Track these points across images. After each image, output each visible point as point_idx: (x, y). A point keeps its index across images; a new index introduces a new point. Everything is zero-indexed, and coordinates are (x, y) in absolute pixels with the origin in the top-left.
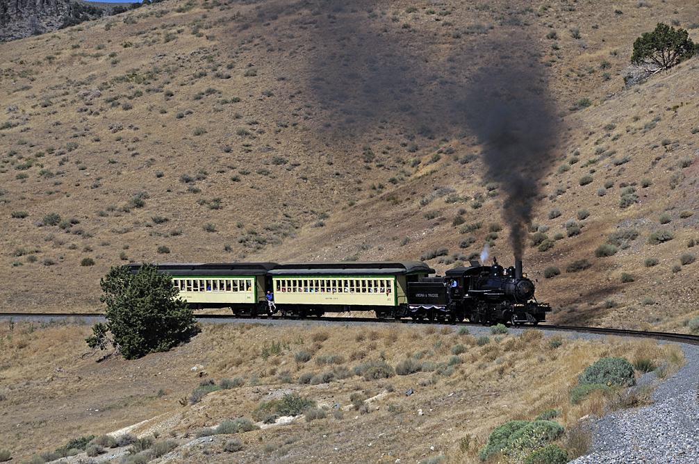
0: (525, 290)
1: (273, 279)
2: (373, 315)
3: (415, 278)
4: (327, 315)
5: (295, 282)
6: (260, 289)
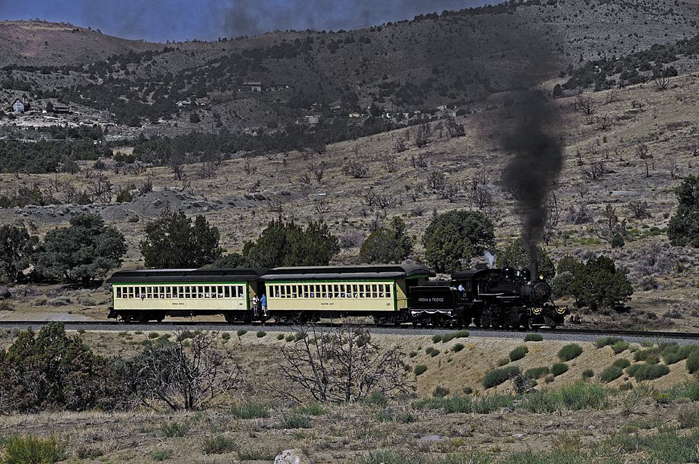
0: (541, 292)
1: (266, 284)
2: (370, 320)
3: (415, 282)
4: (167, 319)
5: (312, 287)
6: (253, 293)
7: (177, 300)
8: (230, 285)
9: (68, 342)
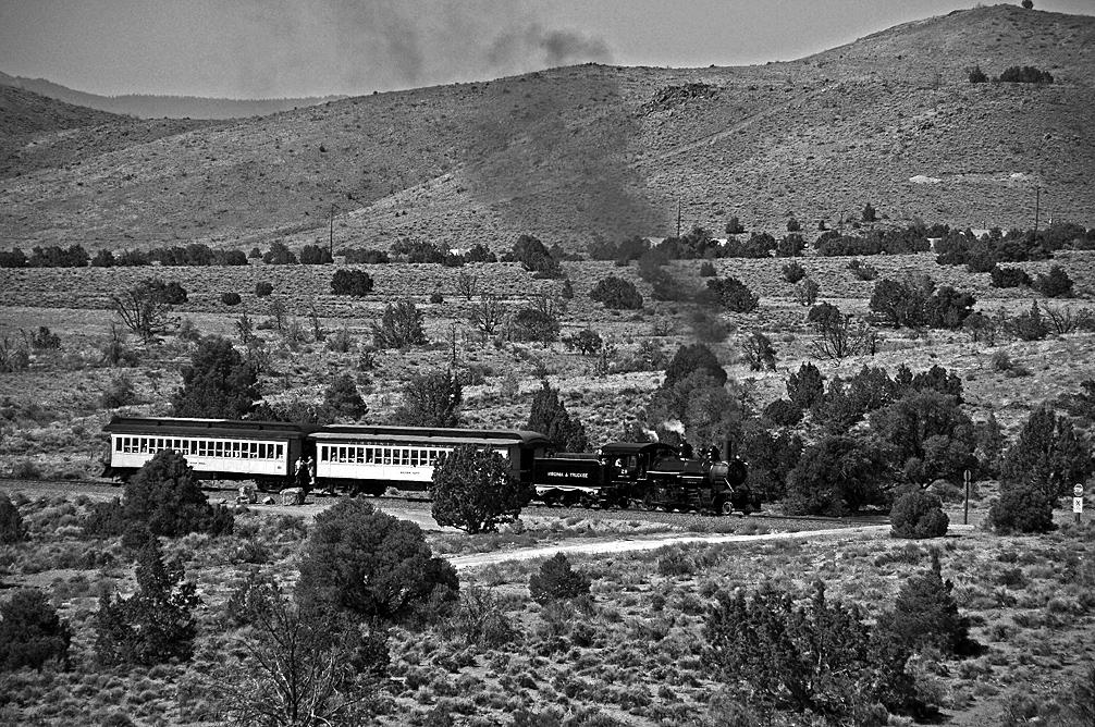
1: (317, 445)
7: (409, 468)
8: (267, 443)
9: (211, 510)
